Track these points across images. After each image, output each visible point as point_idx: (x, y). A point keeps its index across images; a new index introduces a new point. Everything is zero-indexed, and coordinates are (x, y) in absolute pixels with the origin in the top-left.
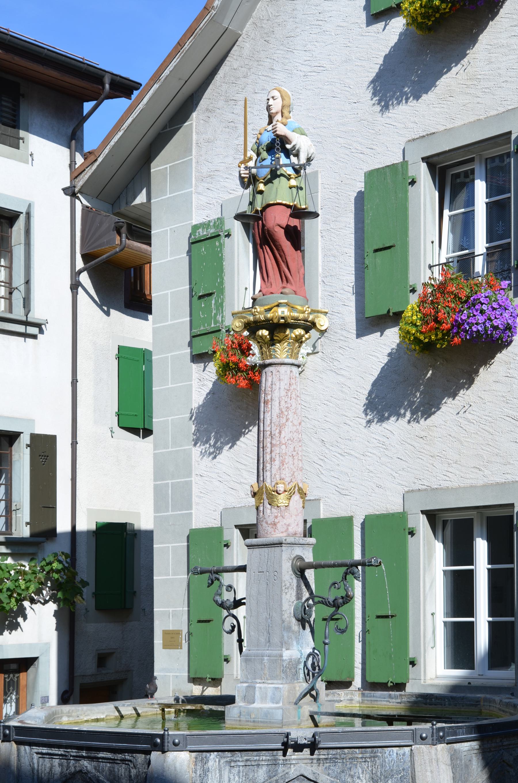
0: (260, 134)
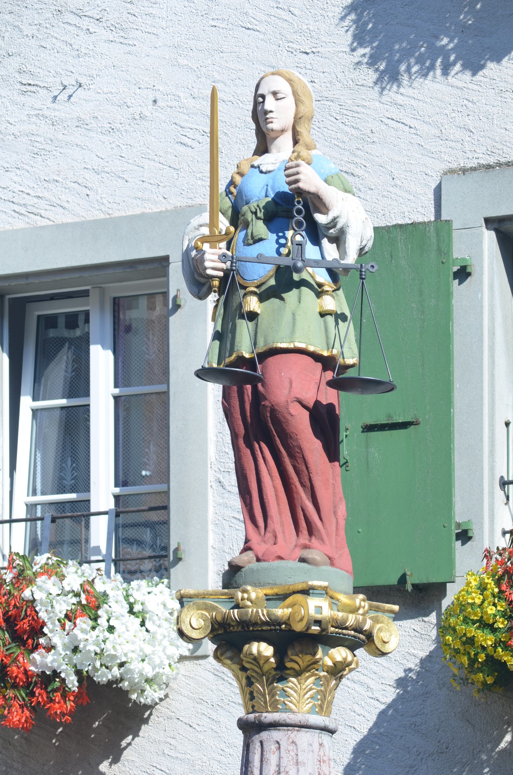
0: (241, 174)
